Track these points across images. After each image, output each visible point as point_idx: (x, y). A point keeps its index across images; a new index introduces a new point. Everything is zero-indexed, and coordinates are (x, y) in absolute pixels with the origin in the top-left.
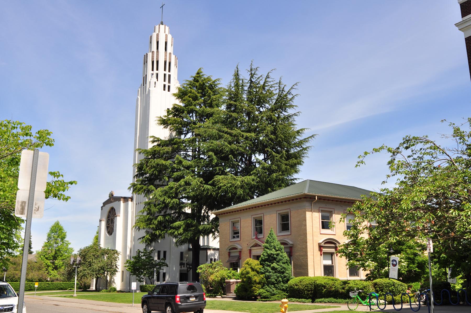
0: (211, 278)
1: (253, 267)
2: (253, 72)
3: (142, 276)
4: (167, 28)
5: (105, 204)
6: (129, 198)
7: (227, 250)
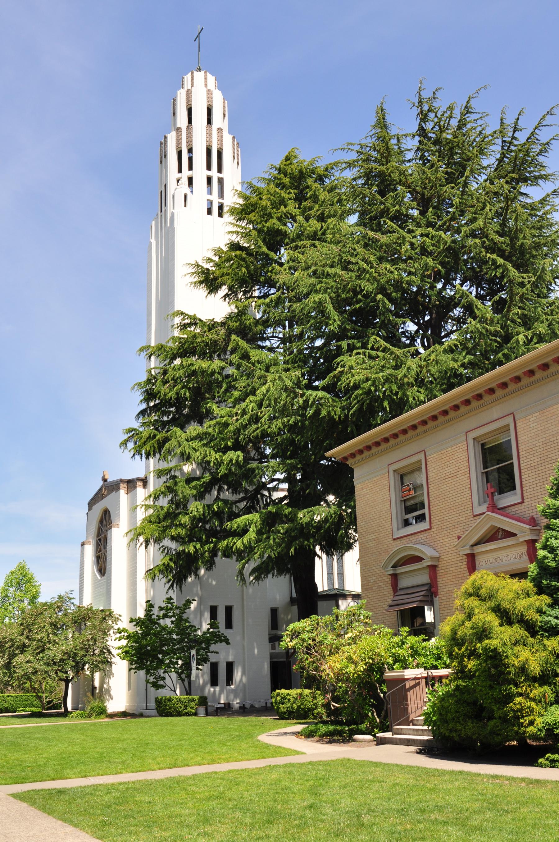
0: (332, 666)
1: (506, 605)
2: (426, 108)
3: (161, 672)
4: (211, 79)
5: (91, 504)
6: (139, 479)
7: (385, 566)
